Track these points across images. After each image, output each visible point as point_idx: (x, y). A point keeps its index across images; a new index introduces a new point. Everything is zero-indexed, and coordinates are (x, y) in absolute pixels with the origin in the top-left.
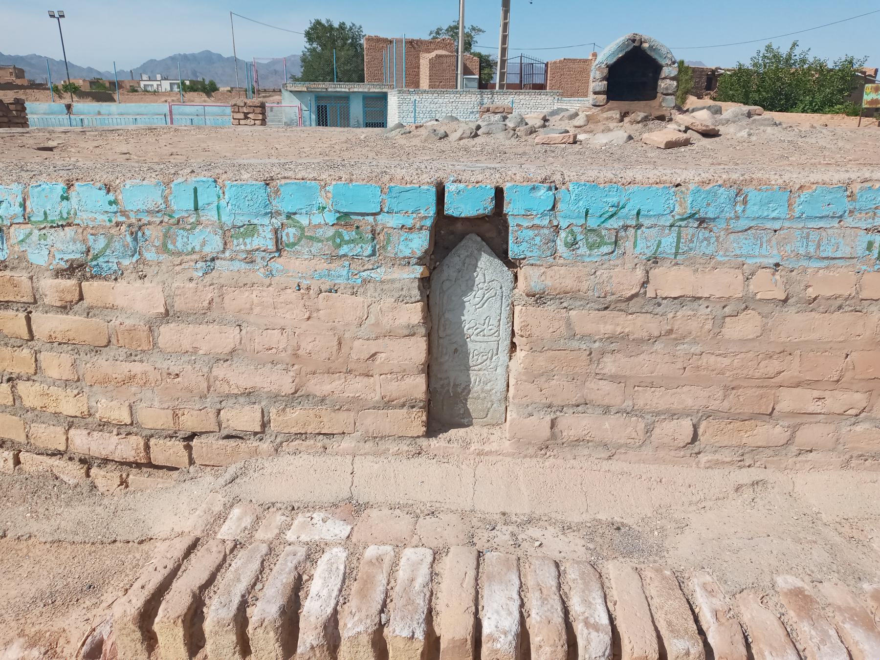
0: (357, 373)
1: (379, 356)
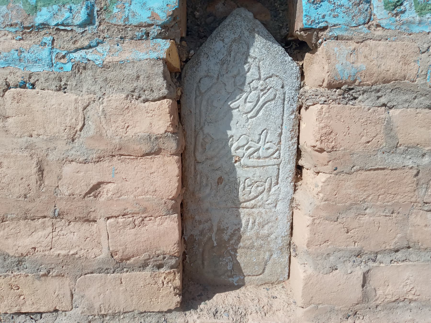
0: (71, 218)
1: (105, 188)
